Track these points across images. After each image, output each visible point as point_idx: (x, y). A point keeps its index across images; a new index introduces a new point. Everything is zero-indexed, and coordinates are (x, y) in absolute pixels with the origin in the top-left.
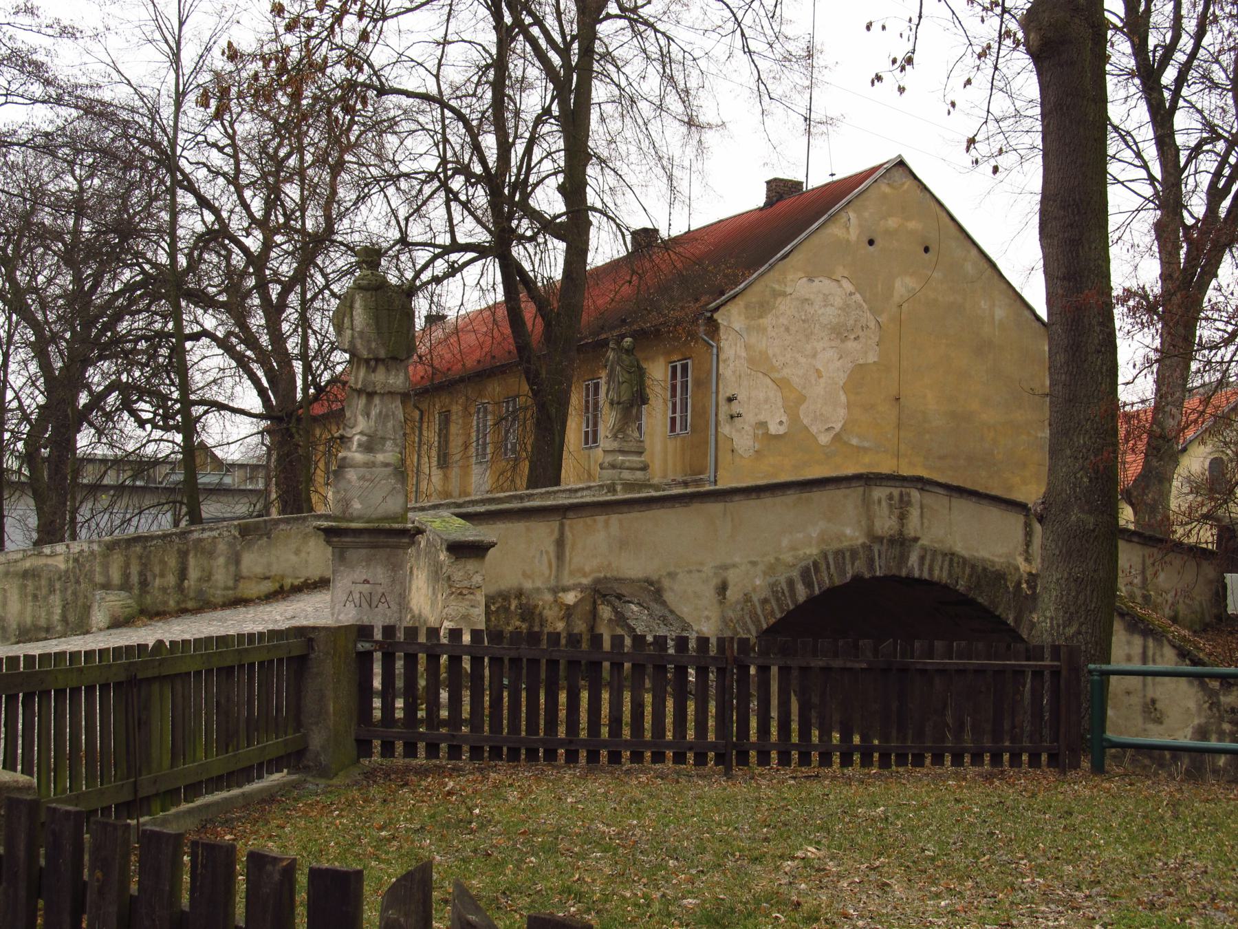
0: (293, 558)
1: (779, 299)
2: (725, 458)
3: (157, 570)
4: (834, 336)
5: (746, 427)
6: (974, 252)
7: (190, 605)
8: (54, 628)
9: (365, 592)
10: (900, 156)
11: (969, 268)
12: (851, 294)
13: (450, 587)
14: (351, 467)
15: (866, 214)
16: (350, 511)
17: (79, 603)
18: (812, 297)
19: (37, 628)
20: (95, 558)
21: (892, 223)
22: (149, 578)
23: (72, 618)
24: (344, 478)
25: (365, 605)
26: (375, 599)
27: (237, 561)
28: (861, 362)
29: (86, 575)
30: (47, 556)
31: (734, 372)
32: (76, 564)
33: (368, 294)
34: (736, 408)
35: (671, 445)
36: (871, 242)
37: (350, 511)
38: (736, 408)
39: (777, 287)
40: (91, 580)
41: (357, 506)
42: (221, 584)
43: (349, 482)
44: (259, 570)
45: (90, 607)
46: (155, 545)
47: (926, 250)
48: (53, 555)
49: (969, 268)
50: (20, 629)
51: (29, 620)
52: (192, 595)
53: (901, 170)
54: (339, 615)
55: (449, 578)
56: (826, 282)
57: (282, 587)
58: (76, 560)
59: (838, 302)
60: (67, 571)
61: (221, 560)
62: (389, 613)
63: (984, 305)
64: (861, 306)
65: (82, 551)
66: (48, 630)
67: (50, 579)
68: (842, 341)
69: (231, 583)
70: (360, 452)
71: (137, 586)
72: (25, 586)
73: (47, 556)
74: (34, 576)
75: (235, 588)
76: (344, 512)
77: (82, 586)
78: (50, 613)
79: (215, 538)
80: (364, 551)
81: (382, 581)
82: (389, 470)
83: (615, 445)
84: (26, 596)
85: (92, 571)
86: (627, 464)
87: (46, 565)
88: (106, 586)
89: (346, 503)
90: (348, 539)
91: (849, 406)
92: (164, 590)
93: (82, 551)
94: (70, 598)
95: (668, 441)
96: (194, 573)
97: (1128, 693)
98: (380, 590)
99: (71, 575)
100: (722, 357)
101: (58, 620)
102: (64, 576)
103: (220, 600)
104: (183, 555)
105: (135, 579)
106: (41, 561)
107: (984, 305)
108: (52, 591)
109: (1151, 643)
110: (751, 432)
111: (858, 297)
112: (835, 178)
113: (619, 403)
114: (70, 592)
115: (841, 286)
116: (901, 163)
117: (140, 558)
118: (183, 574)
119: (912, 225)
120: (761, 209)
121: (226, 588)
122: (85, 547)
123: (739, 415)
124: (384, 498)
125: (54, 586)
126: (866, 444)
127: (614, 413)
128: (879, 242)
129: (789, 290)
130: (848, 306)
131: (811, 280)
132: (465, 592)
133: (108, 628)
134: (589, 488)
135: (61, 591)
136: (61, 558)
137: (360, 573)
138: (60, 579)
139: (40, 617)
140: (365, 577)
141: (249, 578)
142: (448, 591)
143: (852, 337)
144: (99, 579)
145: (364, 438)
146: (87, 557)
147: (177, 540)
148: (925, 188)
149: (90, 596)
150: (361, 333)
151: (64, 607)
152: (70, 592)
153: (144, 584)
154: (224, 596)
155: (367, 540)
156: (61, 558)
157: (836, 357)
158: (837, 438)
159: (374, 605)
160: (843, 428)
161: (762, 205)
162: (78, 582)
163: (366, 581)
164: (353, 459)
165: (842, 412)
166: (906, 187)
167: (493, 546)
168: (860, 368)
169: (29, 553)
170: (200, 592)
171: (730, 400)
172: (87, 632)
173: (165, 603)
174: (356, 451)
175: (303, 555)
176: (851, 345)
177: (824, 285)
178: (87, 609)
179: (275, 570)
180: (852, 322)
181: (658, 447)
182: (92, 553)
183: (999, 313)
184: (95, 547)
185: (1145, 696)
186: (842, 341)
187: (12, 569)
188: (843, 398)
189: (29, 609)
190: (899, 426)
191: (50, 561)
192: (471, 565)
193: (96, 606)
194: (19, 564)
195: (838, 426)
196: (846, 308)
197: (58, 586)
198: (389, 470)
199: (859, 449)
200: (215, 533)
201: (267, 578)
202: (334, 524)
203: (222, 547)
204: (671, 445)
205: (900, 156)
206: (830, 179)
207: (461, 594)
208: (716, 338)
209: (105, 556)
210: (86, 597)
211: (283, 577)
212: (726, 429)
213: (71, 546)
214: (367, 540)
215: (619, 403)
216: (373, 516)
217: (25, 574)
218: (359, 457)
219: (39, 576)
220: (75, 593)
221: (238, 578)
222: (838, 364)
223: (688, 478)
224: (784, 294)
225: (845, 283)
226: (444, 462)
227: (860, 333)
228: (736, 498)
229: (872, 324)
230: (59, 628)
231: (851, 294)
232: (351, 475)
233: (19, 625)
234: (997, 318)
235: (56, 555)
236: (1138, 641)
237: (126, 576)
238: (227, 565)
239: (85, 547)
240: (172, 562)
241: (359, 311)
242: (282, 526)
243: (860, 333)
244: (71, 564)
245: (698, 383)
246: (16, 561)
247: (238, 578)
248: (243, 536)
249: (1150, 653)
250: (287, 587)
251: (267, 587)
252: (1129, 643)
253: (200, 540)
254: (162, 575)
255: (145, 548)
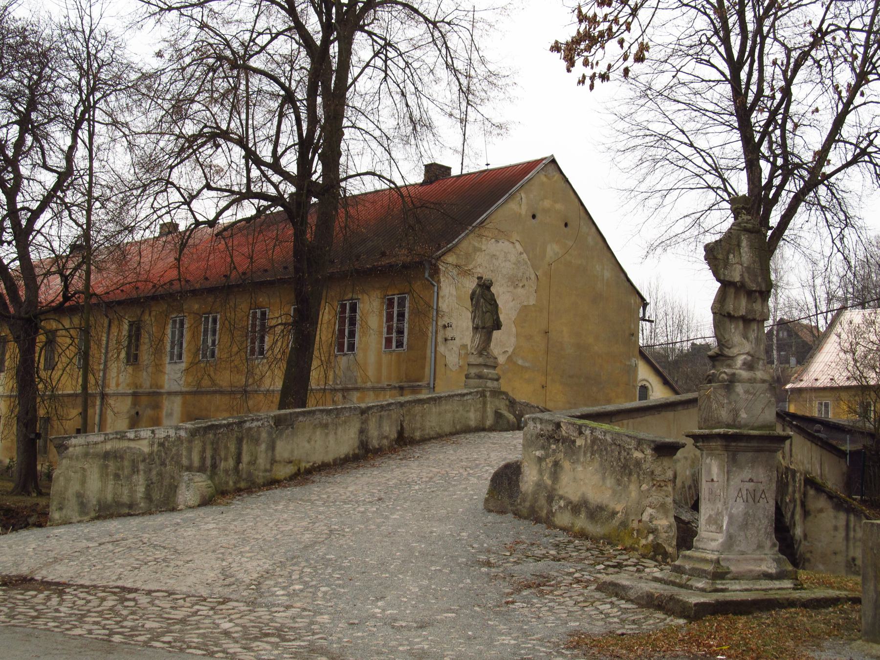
0: (307, 445)
1: (478, 253)
2: (440, 370)
3: (223, 454)
4: (510, 283)
5: (455, 348)
6: (594, 229)
7: (242, 485)
8: (137, 504)
9: (751, 489)
10: (552, 156)
11: (590, 240)
12: (521, 253)
13: (653, 480)
14: (739, 382)
15: (532, 196)
16: (739, 419)
17: (165, 483)
18: (498, 253)
19: (119, 504)
20: (182, 443)
21: (547, 203)
22: (218, 462)
23: (156, 496)
24: (734, 391)
25: (750, 500)
26: (758, 495)
27: (272, 447)
28: (525, 304)
29: (172, 458)
30: (130, 440)
31: (448, 306)
32: (161, 448)
33: (753, 236)
34: (449, 333)
35: (385, 359)
36: (534, 217)
37: (739, 419)
38: (449, 333)
39: (476, 244)
40: (178, 463)
41: (743, 415)
42: (262, 467)
43: (738, 395)
44: (286, 455)
45: (176, 487)
46: (222, 433)
47: (566, 225)
48: (137, 439)
49: (590, 240)
50: (100, 505)
51: (109, 497)
52: (244, 476)
53: (553, 165)
54: (731, 509)
55: (652, 472)
56: (507, 243)
57: (299, 470)
58: (161, 444)
59: (513, 258)
60: (151, 454)
61: (263, 447)
62: (767, 506)
63: (598, 268)
64: (526, 263)
65: (169, 436)
66: (130, 506)
67: (133, 461)
68: (515, 288)
69: (268, 467)
70: (744, 369)
71: (209, 469)
72: (107, 466)
73: (130, 440)
74: (116, 457)
75: (270, 471)
76: (734, 421)
77: (168, 468)
78: (132, 492)
79: (259, 427)
80: (750, 455)
81: (763, 480)
82: (766, 386)
83: (480, 360)
84: (107, 475)
85: (179, 455)
86: (490, 376)
87: (128, 448)
88: (189, 469)
89: (735, 413)
90: (743, 444)
91: (517, 335)
92: (226, 471)
93: (169, 436)
94: (154, 479)
95: (384, 356)
96: (245, 458)
97: (835, 553)
98: (761, 487)
99: (156, 458)
100: (441, 294)
101: (142, 498)
102: (148, 459)
103: (260, 481)
104: (240, 441)
105: (208, 462)
106: (124, 444)
107: (598, 268)
108: (135, 470)
109: (852, 518)
110: (457, 352)
111: (525, 256)
112: (490, 167)
113: (483, 328)
114: (154, 472)
115: (515, 247)
116: (553, 161)
117: (212, 443)
118: (238, 460)
119: (558, 206)
120: (421, 185)
121: (266, 471)
122: (172, 433)
123: (453, 339)
124: (763, 409)
125: (137, 467)
126: (527, 365)
127: (478, 336)
128: (538, 216)
129: (484, 247)
130: (519, 262)
131: (497, 241)
132: (662, 484)
133: (199, 506)
134: (471, 393)
135: (145, 472)
136: (145, 442)
137: (747, 474)
138: (144, 460)
139: (122, 494)
140: (750, 476)
141: (280, 462)
142: (651, 484)
143: (521, 285)
144: (185, 462)
145: (749, 358)
146: (173, 442)
147: (236, 429)
148: (567, 181)
149: (177, 477)
150: (748, 268)
151: (148, 486)
152: (154, 472)
153: (214, 466)
154: (264, 477)
155: (756, 445)
156: (145, 442)
157: (511, 299)
158: (510, 359)
159: (757, 500)
160: (513, 353)
161: (421, 181)
162: (163, 464)
163: (751, 480)
164: (740, 376)
165: (513, 340)
166: (555, 178)
167: (684, 447)
168: (525, 308)
169: (111, 437)
170: (250, 474)
171: (445, 327)
172: (173, 510)
173: (227, 483)
174: (740, 369)
175: (312, 442)
176: (520, 291)
177: (504, 245)
178: (173, 489)
179: (297, 455)
180: (521, 274)
181: (372, 358)
182: (179, 438)
183: (607, 274)
184: (183, 433)
185: (847, 556)
186: (515, 288)
187: (91, 451)
188: (514, 329)
189: (110, 487)
190: (547, 352)
191: (132, 445)
192: (666, 462)
193: (183, 487)
194: (100, 446)
195: (510, 350)
196: (517, 263)
197: (141, 467)
198: (766, 386)
199: (523, 367)
200: (260, 423)
201: (290, 462)
202: (737, 431)
203: (264, 435)
204: (385, 359)
205: (552, 156)
206: (486, 168)
207: (660, 486)
208: (436, 279)
209: (190, 442)
210: (172, 477)
211: (300, 461)
212: (441, 349)
213: (156, 432)
214: (756, 445)
215: (483, 328)
216: (756, 424)
217: (106, 455)
218: (744, 374)
219: (122, 458)
220: (160, 474)
221: (273, 461)
222: (511, 304)
223: (405, 384)
224: (480, 250)
225: (517, 245)
226: (133, 359)
227: (526, 283)
228: (680, 408)
229: (533, 277)
230: (142, 505)
231: (521, 253)
232: (739, 388)
233: (99, 502)
234: (605, 278)
235: (140, 439)
236: (842, 516)
237: (203, 459)
238: (267, 450)
239: (172, 433)
240: (232, 447)
241: (746, 249)
242: (301, 418)
243: (526, 283)
244: (155, 448)
245: (415, 312)
246: (96, 443)
247: (273, 461)
248: (277, 426)
249: (852, 525)
250: (302, 470)
251: (290, 470)
252: (836, 517)
253: (250, 429)
254: (226, 459)
255: (215, 435)
